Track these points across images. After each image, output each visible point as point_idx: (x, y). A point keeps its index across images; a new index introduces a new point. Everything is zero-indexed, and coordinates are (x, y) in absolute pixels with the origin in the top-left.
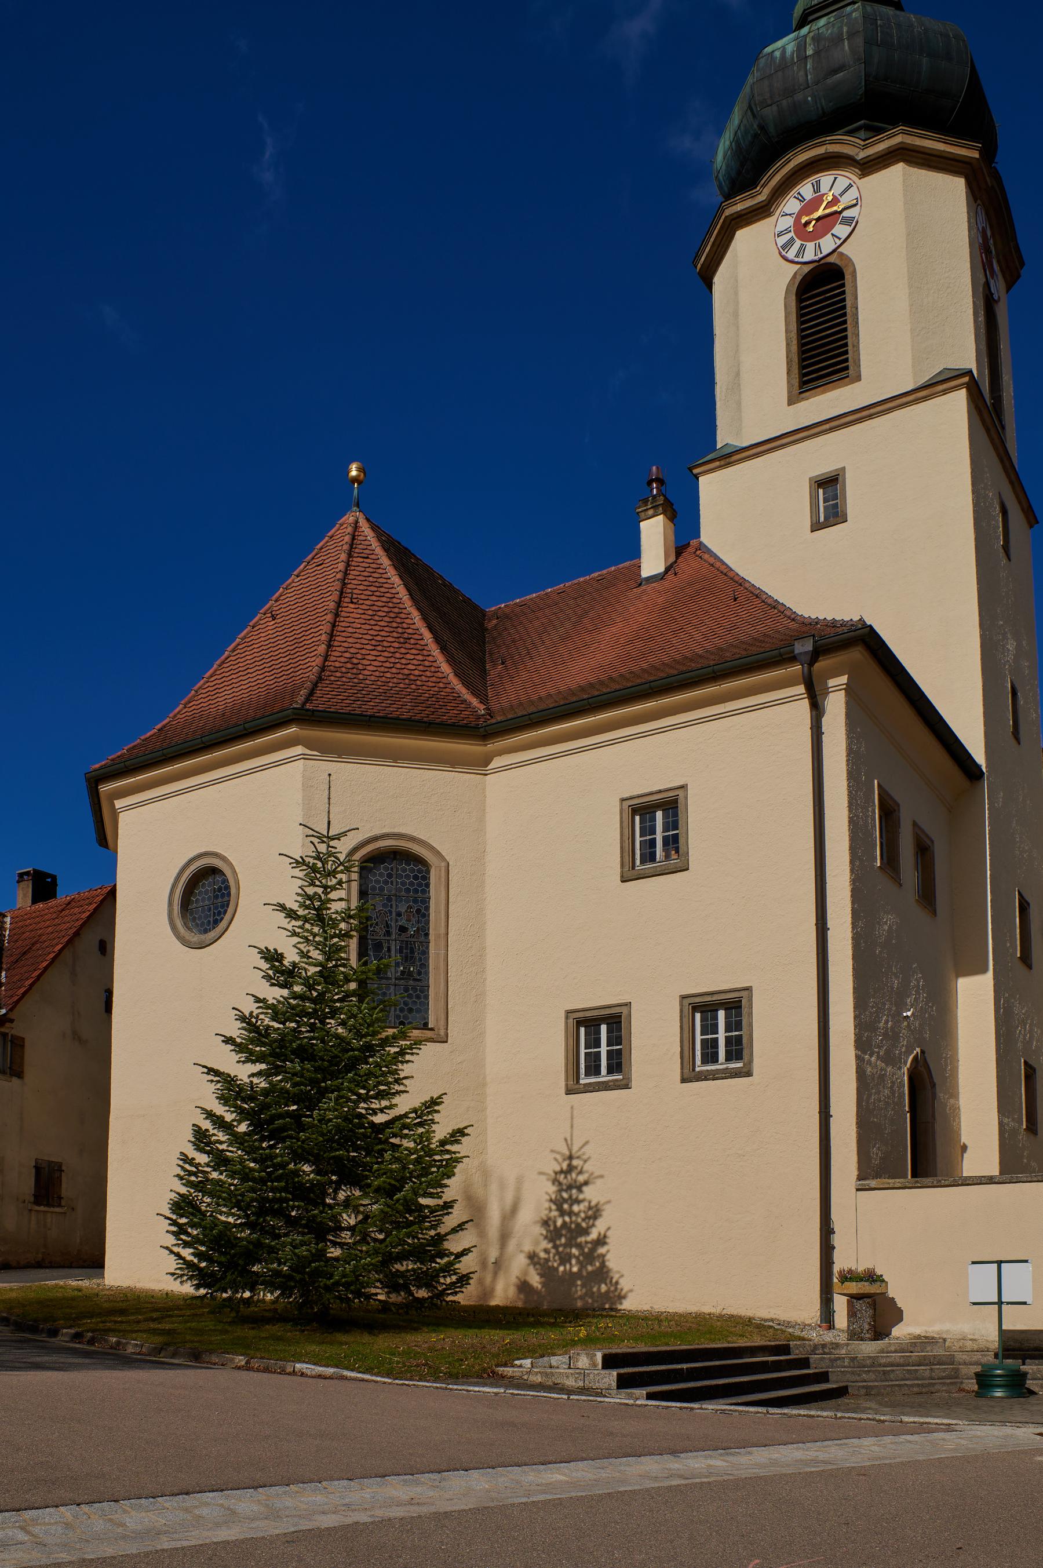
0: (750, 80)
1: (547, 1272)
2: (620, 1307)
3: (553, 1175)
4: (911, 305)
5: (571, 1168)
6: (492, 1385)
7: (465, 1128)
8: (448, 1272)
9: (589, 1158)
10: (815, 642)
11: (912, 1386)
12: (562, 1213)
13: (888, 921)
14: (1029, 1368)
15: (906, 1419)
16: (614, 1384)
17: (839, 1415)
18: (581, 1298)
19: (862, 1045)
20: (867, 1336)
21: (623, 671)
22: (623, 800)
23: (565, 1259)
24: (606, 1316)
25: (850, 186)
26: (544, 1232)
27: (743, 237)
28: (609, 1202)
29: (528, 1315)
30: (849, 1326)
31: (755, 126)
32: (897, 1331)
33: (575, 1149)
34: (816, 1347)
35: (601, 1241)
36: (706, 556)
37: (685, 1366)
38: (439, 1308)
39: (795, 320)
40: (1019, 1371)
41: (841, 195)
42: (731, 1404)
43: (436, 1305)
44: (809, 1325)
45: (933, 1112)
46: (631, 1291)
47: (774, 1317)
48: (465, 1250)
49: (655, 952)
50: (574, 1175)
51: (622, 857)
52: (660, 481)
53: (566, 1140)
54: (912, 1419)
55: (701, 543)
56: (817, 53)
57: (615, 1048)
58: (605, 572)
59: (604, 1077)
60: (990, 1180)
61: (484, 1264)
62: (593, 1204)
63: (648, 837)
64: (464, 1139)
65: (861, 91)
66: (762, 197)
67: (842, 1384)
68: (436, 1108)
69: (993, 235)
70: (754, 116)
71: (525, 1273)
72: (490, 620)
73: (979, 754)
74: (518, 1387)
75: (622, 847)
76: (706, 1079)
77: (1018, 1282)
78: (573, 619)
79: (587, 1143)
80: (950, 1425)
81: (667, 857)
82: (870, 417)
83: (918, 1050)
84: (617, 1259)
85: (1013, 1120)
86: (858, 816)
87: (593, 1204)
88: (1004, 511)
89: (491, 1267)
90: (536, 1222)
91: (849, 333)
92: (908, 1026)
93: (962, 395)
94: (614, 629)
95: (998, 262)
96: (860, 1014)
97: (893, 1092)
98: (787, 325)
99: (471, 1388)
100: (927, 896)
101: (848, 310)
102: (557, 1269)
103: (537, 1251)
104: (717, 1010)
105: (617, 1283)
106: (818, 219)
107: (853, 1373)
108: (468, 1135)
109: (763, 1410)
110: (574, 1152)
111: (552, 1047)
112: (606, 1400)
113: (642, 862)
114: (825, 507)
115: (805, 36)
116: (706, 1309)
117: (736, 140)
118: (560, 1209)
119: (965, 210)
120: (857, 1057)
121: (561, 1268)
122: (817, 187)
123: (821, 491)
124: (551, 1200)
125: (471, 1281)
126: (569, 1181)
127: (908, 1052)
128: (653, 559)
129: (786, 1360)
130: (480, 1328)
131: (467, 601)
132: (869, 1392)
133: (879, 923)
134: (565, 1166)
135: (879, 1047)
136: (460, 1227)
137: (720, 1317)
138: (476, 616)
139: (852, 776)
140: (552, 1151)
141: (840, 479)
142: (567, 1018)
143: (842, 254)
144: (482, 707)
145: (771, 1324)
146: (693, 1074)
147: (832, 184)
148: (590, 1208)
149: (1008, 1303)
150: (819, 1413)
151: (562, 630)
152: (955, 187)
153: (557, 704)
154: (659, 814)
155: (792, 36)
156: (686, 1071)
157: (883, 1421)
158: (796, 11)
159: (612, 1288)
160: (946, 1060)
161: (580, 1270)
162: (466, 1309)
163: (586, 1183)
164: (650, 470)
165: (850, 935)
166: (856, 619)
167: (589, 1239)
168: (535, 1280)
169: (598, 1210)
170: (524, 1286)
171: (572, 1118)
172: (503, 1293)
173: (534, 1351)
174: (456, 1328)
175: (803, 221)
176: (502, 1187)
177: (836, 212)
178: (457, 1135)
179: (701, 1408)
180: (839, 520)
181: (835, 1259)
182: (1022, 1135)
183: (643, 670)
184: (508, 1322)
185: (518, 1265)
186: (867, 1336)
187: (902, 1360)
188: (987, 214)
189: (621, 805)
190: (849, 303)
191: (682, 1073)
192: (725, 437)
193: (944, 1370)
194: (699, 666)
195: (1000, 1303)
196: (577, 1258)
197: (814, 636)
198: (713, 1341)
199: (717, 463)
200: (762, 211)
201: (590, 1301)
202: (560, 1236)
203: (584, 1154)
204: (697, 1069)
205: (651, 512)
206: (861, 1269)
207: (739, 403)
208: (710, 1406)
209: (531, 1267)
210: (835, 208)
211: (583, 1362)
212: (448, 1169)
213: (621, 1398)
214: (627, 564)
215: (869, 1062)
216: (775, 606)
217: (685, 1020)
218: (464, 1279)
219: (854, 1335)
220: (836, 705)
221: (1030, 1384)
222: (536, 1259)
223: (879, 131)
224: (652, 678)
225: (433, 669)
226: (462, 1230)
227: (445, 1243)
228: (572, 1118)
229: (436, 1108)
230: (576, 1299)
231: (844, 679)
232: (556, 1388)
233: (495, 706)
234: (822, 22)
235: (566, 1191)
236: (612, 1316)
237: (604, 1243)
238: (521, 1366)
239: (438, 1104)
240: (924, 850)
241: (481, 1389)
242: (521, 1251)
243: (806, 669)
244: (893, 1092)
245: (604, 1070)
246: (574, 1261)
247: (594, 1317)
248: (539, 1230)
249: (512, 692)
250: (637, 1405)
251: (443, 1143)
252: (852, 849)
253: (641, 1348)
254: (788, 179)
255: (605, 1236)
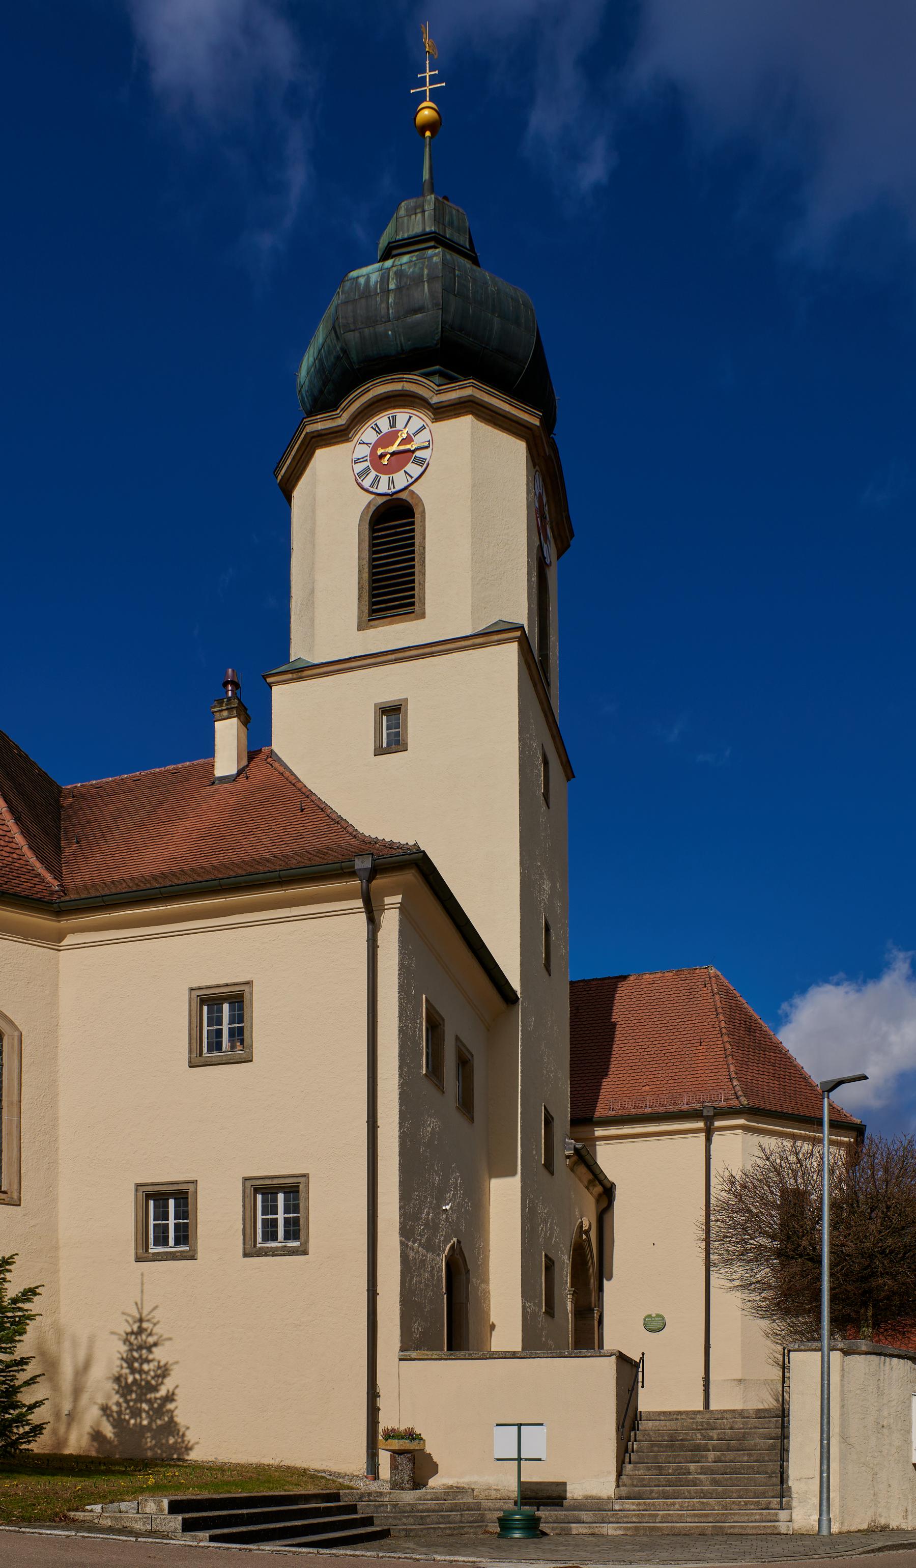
0: (335, 301)
1: (118, 1423)
2: (187, 1458)
3: (124, 1335)
4: (473, 554)
5: (141, 1331)
6: (63, 1528)
7: (37, 1287)
8: (21, 1422)
9: (158, 1322)
10: (373, 860)
11: (445, 1528)
12: (133, 1371)
13: (431, 1124)
14: (543, 1513)
15: (438, 1557)
16: (180, 1528)
17: (381, 1554)
18: (151, 1448)
19: (406, 1232)
20: (407, 1486)
21: (194, 865)
22: (192, 989)
23: (136, 1413)
24: (174, 1466)
25: (423, 428)
26: (116, 1387)
27: (323, 457)
28: (177, 1363)
29: (100, 1464)
30: (391, 1477)
31: (338, 349)
32: (433, 1482)
33: (145, 1313)
34: (362, 1495)
35: (170, 1398)
36: (276, 765)
37: (245, 1511)
38: (13, 1456)
39: (367, 548)
40: (534, 1516)
41: (416, 434)
42: (286, 1546)
43: (9, 1453)
44: (357, 1476)
45: (467, 1294)
46: (197, 1443)
47: (326, 1468)
48: (37, 1402)
49: (218, 1133)
50: (144, 1337)
51: (190, 1043)
52: (236, 685)
53: (136, 1304)
54: (443, 1558)
55: (272, 751)
56: (399, 289)
57: (182, 1221)
58: (179, 766)
59: (171, 1247)
60: (513, 1355)
61: (57, 1415)
62: (162, 1364)
63: (215, 1027)
64: (36, 1298)
65: (438, 337)
66: (342, 421)
67: (384, 1528)
68: (8, 1267)
69: (548, 501)
70: (337, 338)
71: (98, 1423)
72: (66, 798)
73: (515, 983)
74: (89, 1530)
75: (190, 1034)
76: (266, 1255)
77: (535, 1442)
78: (148, 808)
79: (156, 1307)
80: (475, 1562)
81: (233, 1047)
82: (432, 654)
83: (455, 1239)
84: (183, 1413)
85: (535, 1304)
86: (407, 1027)
87: (162, 1364)
88: (546, 762)
89: (64, 1419)
90: (108, 1378)
91: (417, 570)
92: (447, 1218)
93: (513, 649)
94: (187, 824)
95: (552, 528)
96: (405, 1205)
97: (432, 1276)
98: (360, 551)
99: (43, 1531)
100: (466, 1104)
101: (417, 548)
102: (128, 1422)
103: (110, 1404)
104: (277, 1193)
105: (183, 1435)
106: (393, 454)
107: (395, 1518)
108: (39, 1294)
109: (315, 1550)
110: (144, 1315)
111: (122, 1218)
112: (172, 1542)
113: (209, 1050)
114: (388, 734)
115: (389, 269)
116: (266, 1461)
117: (319, 359)
118: (131, 1367)
119: (525, 473)
120: (402, 1243)
121: (132, 1421)
122: (393, 422)
123: (385, 718)
124: (122, 1359)
125: (44, 1431)
126: (139, 1342)
127: (446, 1241)
128: (227, 757)
129: (337, 1507)
130: (53, 1475)
131: (44, 775)
132: (408, 1534)
133: (423, 1125)
134: (135, 1327)
135: (421, 1236)
136: (32, 1381)
137: (278, 1468)
138: (53, 791)
139: (403, 989)
140: (123, 1313)
141: (403, 709)
142: (137, 1190)
143: (413, 492)
144: (56, 883)
145: (323, 1474)
146: (254, 1250)
147: (409, 421)
148: (159, 1367)
149: (526, 1460)
150: (363, 1553)
151: (136, 818)
152: (516, 449)
153: (130, 890)
154: (226, 1007)
155: (377, 266)
156: (248, 1247)
157: (419, 1560)
158: (381, 241)
159: (180, 1440)
160: (479, 1251)
161: (150, 1423)
162: (39, 1457)
163: (155, 1344)
164: (226, 672)
165: (397, 1134)
166: (411, 843)
167: (158, 1395)
168: (108, 1431)
169: (166, 1370)
170: (97, 1436)
171: (142, 1284)
172: (77, 1442)
173: (105, 1497)
174: (30, 1475)
175: (379, 453)
176: (75, 1344)
177: (409, 451)
178: (30, 1293)
179: (259, 1549)
180: (401, 748)
181: (380, 1420)
182: (542, 1318)
183: (214, 867)
184: (80, 1470)
185: (91, 1416)
186: (407, 1486)
187: (437, 1507)
188: (543, 481)
189: (190, 994)
190: (417, 541)
191: (244, 1249)
192: (298, 651)
193: (472, 1515)
194: (266, 869)
195: (519, 1459)
196: (147, 1412)
197: (372, 854)
198: (271, 1489)
199: (290, 676)
200: (340, 435)
201: (159, 1451)
202: (131, 1392)
203: (153, 1318)
204: (258, 1246)
205: (225, 713)
206: (402, 1428)
207: (312, 620)
208: (267, 1547)
209: (104, 1418)
210: (408, 447)
211: (151, 1507)
212: (20, 1325)
213: (187, 1540)
214: (201, 761)
215: (412, 1248)
216: (338, 821)
217: (248, 1200)
218: (37, 1429)
219: (396, 1485)
220: (390, 921)
221: (543, 1526)
222: (108, 1412)
223: (453, 380)
224: (221, 876)
225: (7, 839)
226: (34, 1383)
227: (19, 1395)
228: (142, 1284)
229: (8, 1267)
230: (146, 1450)
231: (398, 898)
232: (125, 1531)
233: (70, 885)
234: (405, 259)
235: (136, 1351)
236: (179, 1466)
237: (172, 1400)
238: (91, 1511)
239: (10, 1264)
240: (464, 1062)
241: (53, 1532)
242: (95, 1403)
243: (364, 885)
244: (432, 1276)
245: (171, 1241)
246: (144, 1415)
247: (162, 1466)
248: (111, 1386)
249: (87, 871)
250: (199, 1547)
251: (14, 1301)
252: (402, 1056)
253: (206, 1495)
254: (366, 408)
255: (173, 1394)
